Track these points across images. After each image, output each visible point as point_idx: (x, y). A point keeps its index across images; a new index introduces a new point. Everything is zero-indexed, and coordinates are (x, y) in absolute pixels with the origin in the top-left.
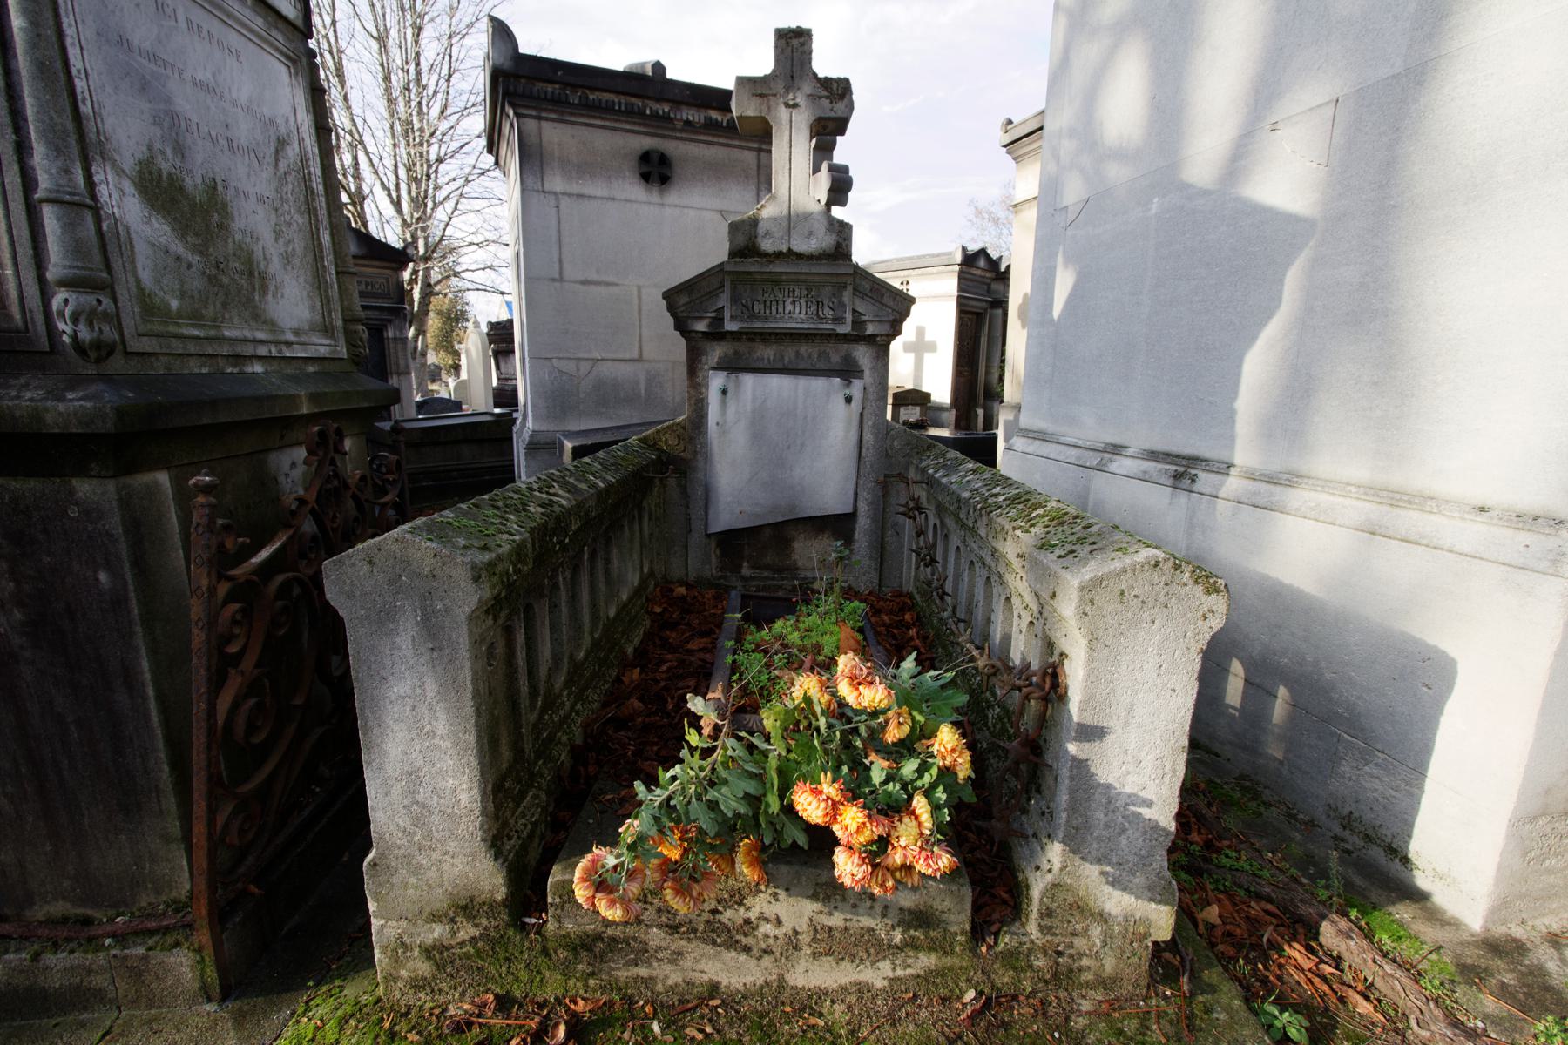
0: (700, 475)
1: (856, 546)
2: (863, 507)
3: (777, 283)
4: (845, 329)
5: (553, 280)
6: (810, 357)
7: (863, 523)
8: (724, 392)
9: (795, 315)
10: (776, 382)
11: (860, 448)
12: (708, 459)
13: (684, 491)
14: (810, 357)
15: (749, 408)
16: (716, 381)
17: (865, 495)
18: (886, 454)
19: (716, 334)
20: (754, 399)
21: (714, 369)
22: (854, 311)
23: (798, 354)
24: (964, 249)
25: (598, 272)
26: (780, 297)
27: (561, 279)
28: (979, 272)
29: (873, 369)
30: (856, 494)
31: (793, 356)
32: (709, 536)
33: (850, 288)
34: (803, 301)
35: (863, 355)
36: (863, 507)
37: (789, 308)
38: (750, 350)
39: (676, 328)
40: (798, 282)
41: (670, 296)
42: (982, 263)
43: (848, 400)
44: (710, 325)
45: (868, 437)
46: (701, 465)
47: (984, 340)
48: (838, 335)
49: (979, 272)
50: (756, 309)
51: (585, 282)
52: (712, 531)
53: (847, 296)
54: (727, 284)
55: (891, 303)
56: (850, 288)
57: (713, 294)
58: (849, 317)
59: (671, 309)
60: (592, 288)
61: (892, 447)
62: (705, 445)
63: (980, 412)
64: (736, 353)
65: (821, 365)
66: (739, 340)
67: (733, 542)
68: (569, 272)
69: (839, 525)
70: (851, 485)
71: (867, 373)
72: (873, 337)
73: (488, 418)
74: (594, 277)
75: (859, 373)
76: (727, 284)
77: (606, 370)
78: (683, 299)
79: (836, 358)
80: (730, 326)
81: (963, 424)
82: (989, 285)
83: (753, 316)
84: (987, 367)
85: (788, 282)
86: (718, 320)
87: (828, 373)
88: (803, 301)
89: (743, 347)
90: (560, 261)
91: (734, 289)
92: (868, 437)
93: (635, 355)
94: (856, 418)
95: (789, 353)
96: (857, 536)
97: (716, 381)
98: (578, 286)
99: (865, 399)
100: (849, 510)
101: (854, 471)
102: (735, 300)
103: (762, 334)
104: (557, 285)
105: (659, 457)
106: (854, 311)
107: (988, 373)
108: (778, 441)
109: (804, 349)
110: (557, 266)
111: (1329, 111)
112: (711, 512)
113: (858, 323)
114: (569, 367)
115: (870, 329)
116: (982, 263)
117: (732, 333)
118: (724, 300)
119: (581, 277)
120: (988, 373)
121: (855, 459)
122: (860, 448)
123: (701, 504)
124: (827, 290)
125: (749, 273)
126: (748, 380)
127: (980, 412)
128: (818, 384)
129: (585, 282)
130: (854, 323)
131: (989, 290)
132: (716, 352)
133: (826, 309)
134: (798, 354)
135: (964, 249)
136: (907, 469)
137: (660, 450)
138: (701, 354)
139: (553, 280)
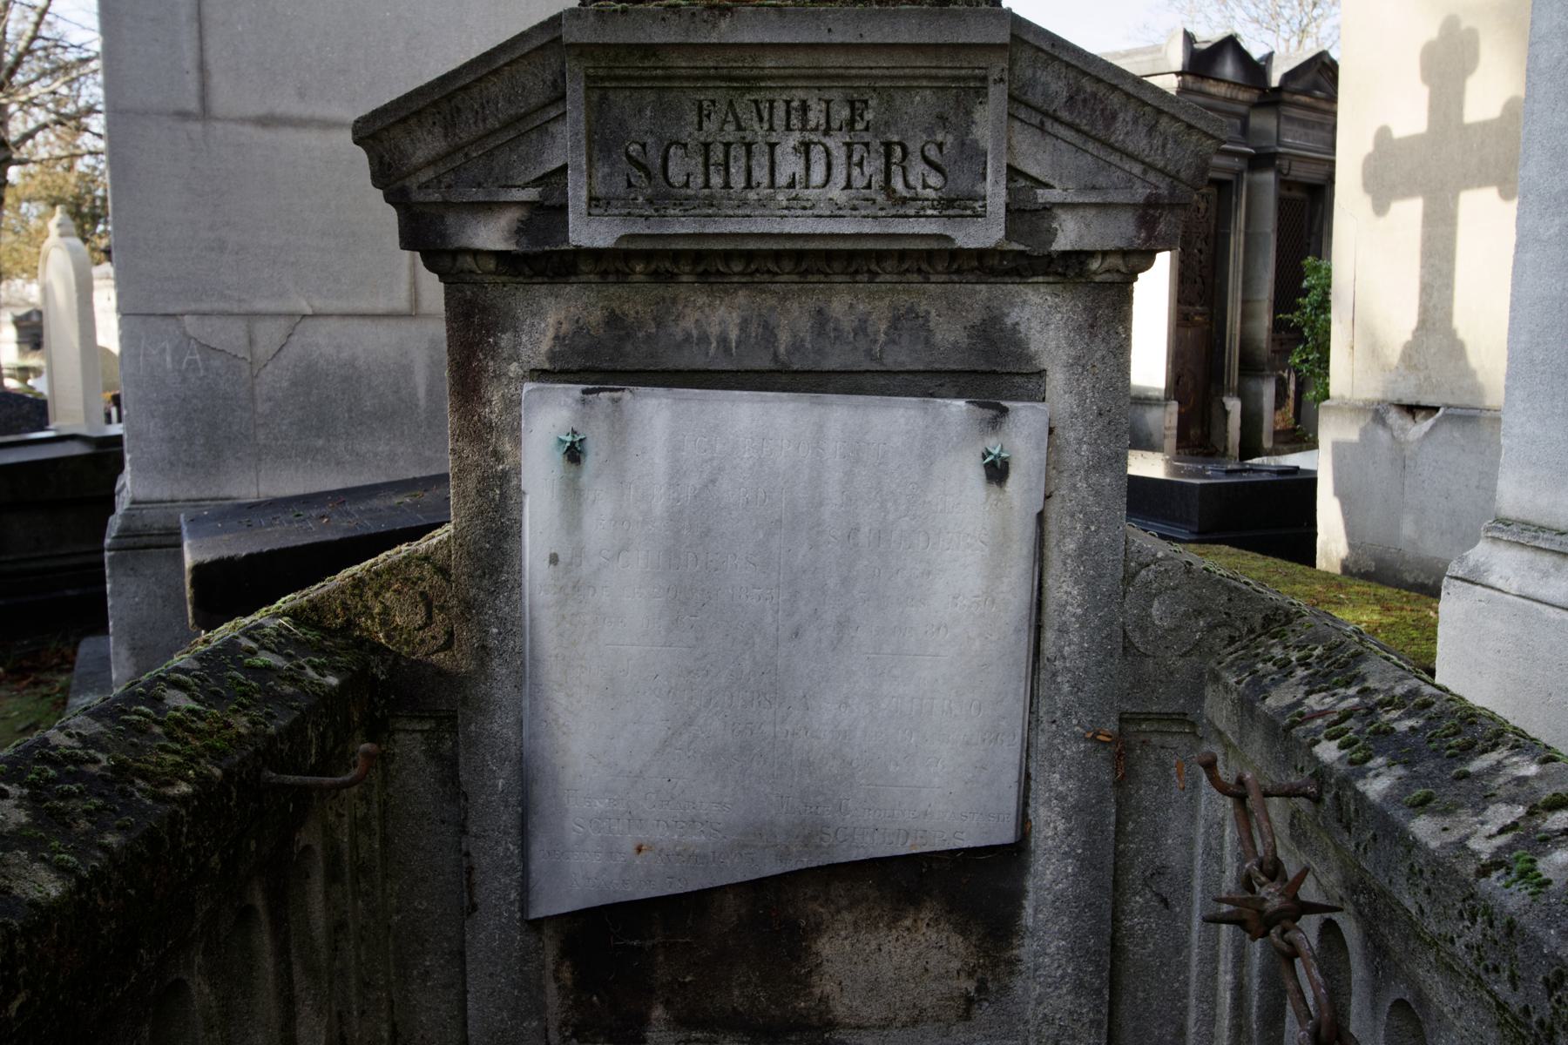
0: (501, 725)
1: (1026, 950)
2: (1049, 824)
3: (749, 83)
4: (984, 233)
5: (184, 115)
6: (861, 329)
7: (1049, 874)
8: (574, 453)
9: (812, 190)
10: (745, 413)
11: (1038, 629)
12: (523, 673)
13: (449, 769)
14: (861, 329)
15: (659, 506)
16: (546, 418)
17: (1053, 782)
18: (1124, 647)
19: (544, 261)
20: (676, 475)
21: (540, 375)
22: (1013, 172)
23: (821, 317)
24: (1189, 38)
25: (301, 95)
26: (757, 131)
27: (205, 113)
28: (1221, 90)
29: (1077, 364)
30: (1026, 779)
31: (805, 324)
32: (537, 925)
33: (997, 95)
34: (835, 143)
35: (1042, 320)
36: (1049, 824)
37: (790, 164)
38: (665, 307)
39: (409, 240)
40: (818, 78)
41: (379, 133)
42: (1229, 69)
43: (997, 472)
44: (522, 230)
45: (1063, 590)
46: (501, 690)
47: (1236, 243)
48: (956, 254)
49: (1221, 90)
50: (676, 173)
51: (267, 121)
52: (540, 910)
53: (987, 123)
54: (575, 92)
55: (1138, 142)
56: (997, 95)
57: (529, 125)
58: (995, 193)
59: (387, 176)
60: (287, 136)
61: (1143, 623)
62: (513, 626)
63: (1234, 405)
64: (614, 320)
65: (901, 357)
66: (622, 277)
67: (618, 946)
68: (224, 97)
69: (970, 886)
70: (1010, 755)
71: (1057, 380)
72: (1076, 259)
73: (77, 449)
74: (288, 105)
75: (1030, 382)
76: (575, 92)
77: (323, 340)
78: (426, 145)
79: (949, 333)
80: (588, 232)
81: (1194, 432)
82: (1245, 119)
83: (665, 198)
84: (1245, 302)
85: (787, 79)
86: (547, 213)
87: (925, 382)
88: (835, 143)
89: (635, 301)
90: (202, 68)
91: (598, 110)
92: (1063, 590)
93: (401, 302)
94: (1023, 531)
95: (792, 317)
96: (1028, 917)
97: (546, 418)
98: (249, 130)
99: (1053, 463)
100: (1007, 836)
101: (1021, 688)
102: (601, 143)
103: (698, 256)
104: (196, 128)
105: (358, 680)
106: (1013, 172)
107: (1246, 316)
108: (754, 613)
109: (844, 303)
110: (192, 85)
111: (1017, 124)
112: (539, 849)
113: (1026, 214)
114: (229, 335)
115: (1068, 234)
116: (1229, 69)
117: (596, 254)
118: (565, 146)
119: (255, 109)
120: (1246, 316)
121: (1023, 667)
122: (1038, 629)
123: (507, 818)
124: (920, 104)
125: (650, 50)
126: (656, 413)
127: (1234, 405)
128: (894, 421)
129: (267, 121)
130: (1015, 213)
131: (1245, 129)
132: (546, 320)
133: (918, 169)
134: (821, 317)
135: (1189, 38)
136: (1197, 696)
137: (367, 646)
138: (492, 328)
139: (184, 115)
